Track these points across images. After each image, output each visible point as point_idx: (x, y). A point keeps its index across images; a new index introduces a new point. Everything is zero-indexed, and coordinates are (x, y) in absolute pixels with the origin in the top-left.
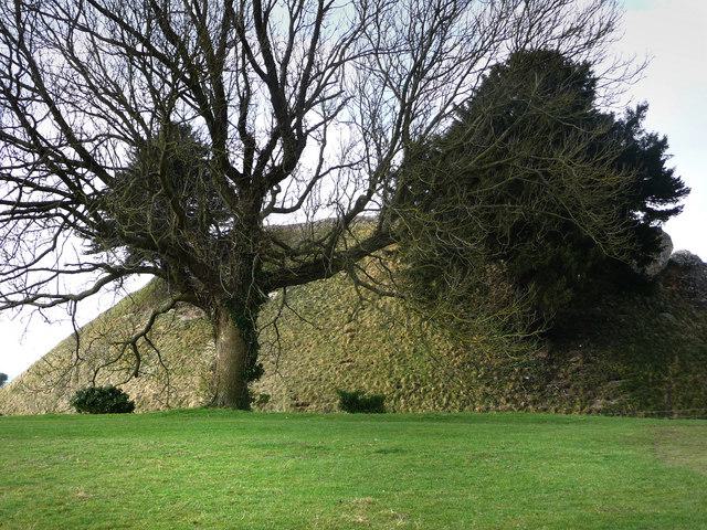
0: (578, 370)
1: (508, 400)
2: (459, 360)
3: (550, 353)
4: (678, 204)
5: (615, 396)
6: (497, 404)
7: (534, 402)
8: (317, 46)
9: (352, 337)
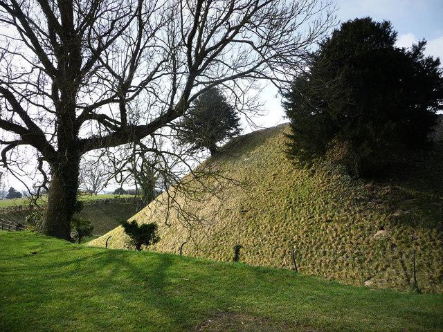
0: (388, 193)
1: (345, 211)
2: (323, 189)
3: (373, 184)
4: (116, 195)
5: (408, 209)
6: (339, 212)
7: (360, 211)
8: (171, 94)
9: (274, 178)
